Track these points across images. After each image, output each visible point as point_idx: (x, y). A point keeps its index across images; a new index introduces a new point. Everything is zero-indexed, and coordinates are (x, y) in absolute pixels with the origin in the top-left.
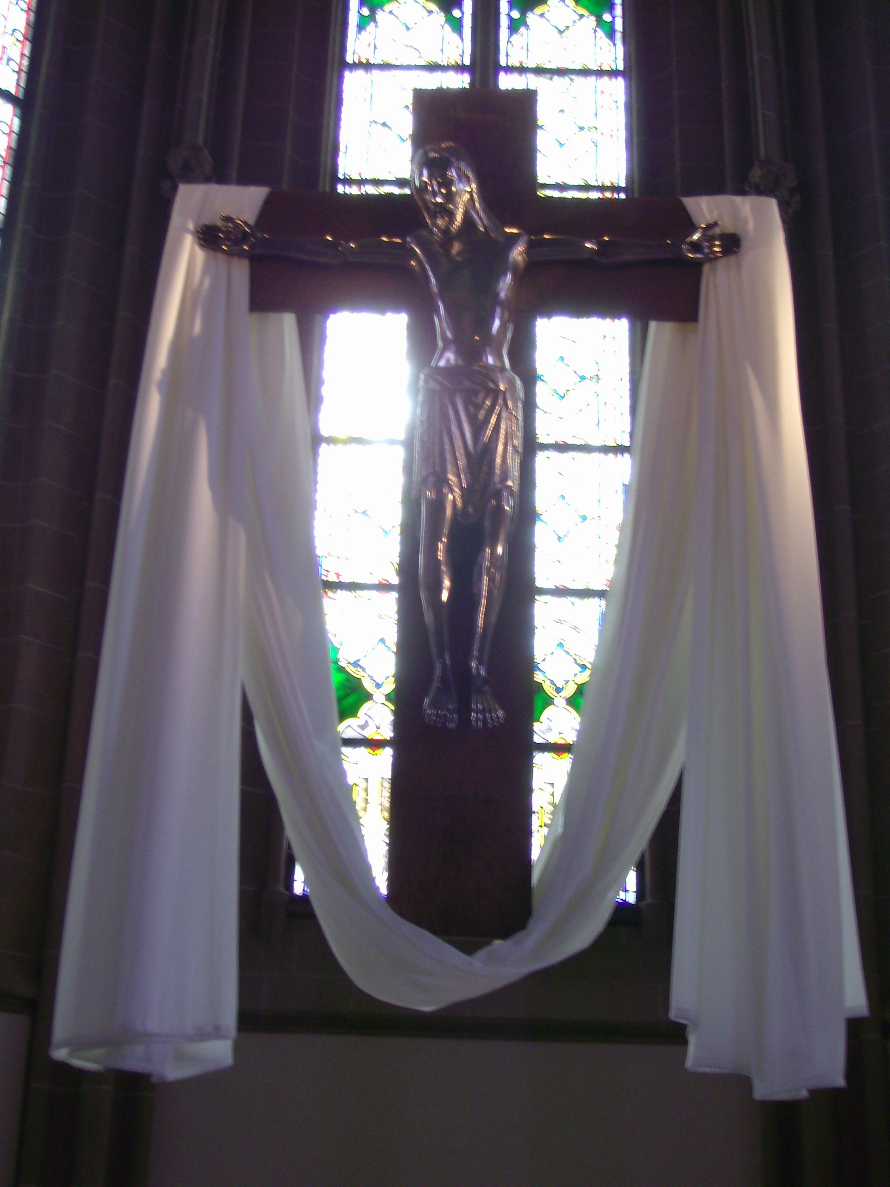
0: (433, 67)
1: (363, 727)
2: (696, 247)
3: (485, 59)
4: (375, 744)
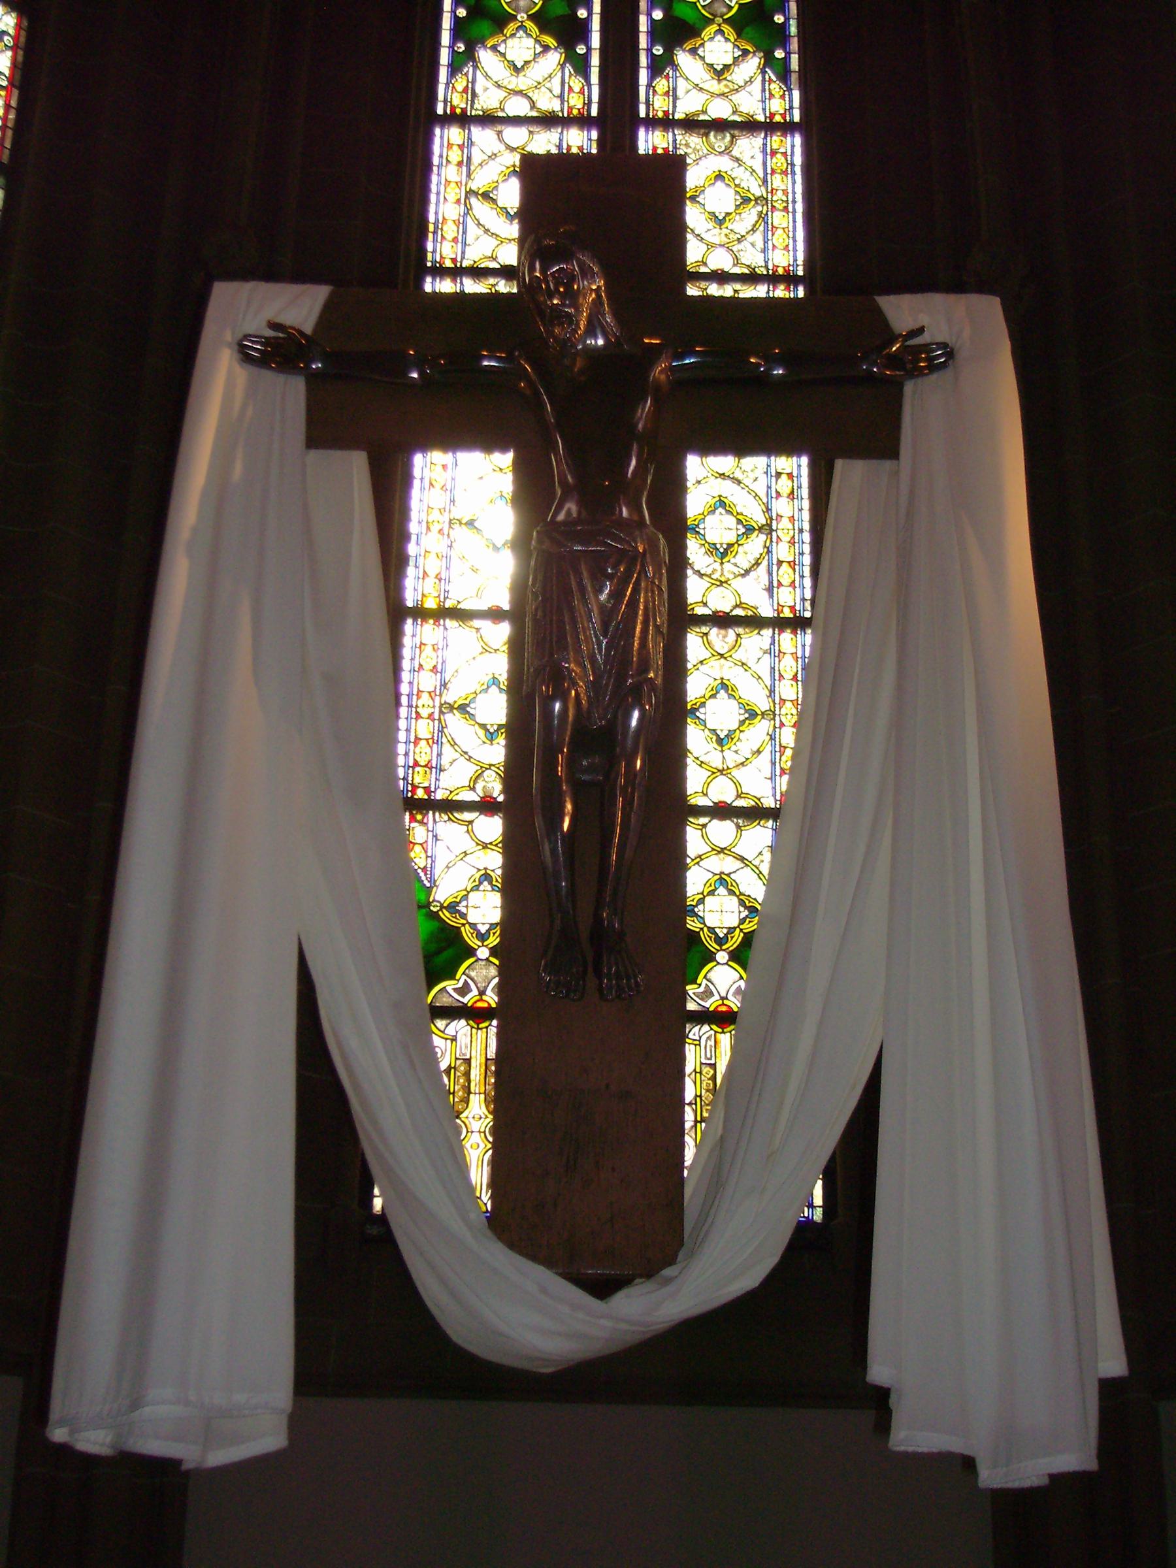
0: (548, 120)
1: (464, 990)
3: (618, 113)
4: (476, 1015)
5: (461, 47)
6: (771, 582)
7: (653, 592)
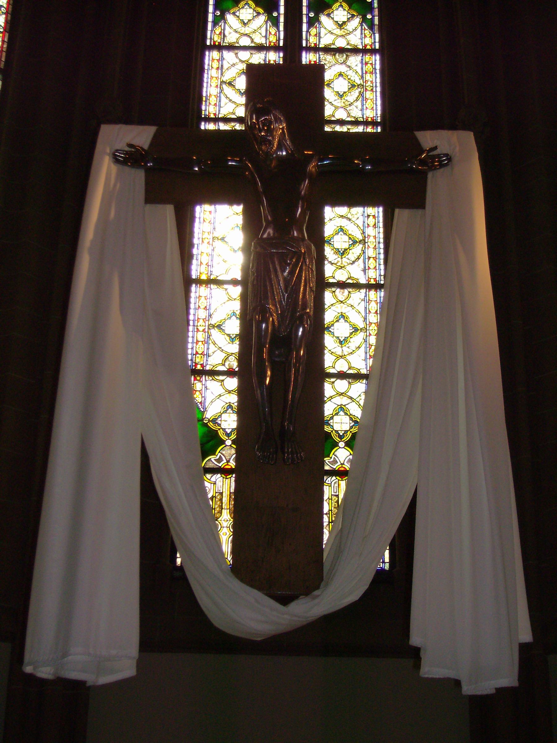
0: (260, 48)
2: (423, 162)
3: (293, 45)
4: (225, 472)
5: (218, 13)
6: (365, 267)
7: (309, 271)
